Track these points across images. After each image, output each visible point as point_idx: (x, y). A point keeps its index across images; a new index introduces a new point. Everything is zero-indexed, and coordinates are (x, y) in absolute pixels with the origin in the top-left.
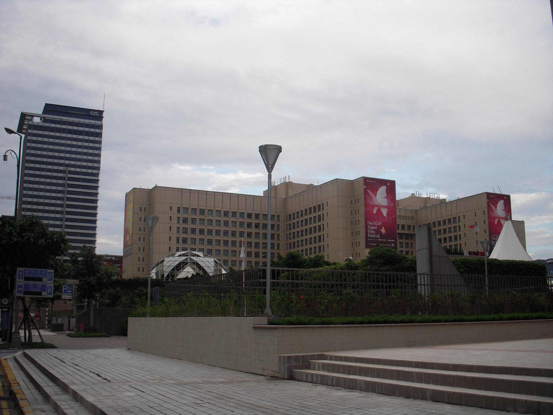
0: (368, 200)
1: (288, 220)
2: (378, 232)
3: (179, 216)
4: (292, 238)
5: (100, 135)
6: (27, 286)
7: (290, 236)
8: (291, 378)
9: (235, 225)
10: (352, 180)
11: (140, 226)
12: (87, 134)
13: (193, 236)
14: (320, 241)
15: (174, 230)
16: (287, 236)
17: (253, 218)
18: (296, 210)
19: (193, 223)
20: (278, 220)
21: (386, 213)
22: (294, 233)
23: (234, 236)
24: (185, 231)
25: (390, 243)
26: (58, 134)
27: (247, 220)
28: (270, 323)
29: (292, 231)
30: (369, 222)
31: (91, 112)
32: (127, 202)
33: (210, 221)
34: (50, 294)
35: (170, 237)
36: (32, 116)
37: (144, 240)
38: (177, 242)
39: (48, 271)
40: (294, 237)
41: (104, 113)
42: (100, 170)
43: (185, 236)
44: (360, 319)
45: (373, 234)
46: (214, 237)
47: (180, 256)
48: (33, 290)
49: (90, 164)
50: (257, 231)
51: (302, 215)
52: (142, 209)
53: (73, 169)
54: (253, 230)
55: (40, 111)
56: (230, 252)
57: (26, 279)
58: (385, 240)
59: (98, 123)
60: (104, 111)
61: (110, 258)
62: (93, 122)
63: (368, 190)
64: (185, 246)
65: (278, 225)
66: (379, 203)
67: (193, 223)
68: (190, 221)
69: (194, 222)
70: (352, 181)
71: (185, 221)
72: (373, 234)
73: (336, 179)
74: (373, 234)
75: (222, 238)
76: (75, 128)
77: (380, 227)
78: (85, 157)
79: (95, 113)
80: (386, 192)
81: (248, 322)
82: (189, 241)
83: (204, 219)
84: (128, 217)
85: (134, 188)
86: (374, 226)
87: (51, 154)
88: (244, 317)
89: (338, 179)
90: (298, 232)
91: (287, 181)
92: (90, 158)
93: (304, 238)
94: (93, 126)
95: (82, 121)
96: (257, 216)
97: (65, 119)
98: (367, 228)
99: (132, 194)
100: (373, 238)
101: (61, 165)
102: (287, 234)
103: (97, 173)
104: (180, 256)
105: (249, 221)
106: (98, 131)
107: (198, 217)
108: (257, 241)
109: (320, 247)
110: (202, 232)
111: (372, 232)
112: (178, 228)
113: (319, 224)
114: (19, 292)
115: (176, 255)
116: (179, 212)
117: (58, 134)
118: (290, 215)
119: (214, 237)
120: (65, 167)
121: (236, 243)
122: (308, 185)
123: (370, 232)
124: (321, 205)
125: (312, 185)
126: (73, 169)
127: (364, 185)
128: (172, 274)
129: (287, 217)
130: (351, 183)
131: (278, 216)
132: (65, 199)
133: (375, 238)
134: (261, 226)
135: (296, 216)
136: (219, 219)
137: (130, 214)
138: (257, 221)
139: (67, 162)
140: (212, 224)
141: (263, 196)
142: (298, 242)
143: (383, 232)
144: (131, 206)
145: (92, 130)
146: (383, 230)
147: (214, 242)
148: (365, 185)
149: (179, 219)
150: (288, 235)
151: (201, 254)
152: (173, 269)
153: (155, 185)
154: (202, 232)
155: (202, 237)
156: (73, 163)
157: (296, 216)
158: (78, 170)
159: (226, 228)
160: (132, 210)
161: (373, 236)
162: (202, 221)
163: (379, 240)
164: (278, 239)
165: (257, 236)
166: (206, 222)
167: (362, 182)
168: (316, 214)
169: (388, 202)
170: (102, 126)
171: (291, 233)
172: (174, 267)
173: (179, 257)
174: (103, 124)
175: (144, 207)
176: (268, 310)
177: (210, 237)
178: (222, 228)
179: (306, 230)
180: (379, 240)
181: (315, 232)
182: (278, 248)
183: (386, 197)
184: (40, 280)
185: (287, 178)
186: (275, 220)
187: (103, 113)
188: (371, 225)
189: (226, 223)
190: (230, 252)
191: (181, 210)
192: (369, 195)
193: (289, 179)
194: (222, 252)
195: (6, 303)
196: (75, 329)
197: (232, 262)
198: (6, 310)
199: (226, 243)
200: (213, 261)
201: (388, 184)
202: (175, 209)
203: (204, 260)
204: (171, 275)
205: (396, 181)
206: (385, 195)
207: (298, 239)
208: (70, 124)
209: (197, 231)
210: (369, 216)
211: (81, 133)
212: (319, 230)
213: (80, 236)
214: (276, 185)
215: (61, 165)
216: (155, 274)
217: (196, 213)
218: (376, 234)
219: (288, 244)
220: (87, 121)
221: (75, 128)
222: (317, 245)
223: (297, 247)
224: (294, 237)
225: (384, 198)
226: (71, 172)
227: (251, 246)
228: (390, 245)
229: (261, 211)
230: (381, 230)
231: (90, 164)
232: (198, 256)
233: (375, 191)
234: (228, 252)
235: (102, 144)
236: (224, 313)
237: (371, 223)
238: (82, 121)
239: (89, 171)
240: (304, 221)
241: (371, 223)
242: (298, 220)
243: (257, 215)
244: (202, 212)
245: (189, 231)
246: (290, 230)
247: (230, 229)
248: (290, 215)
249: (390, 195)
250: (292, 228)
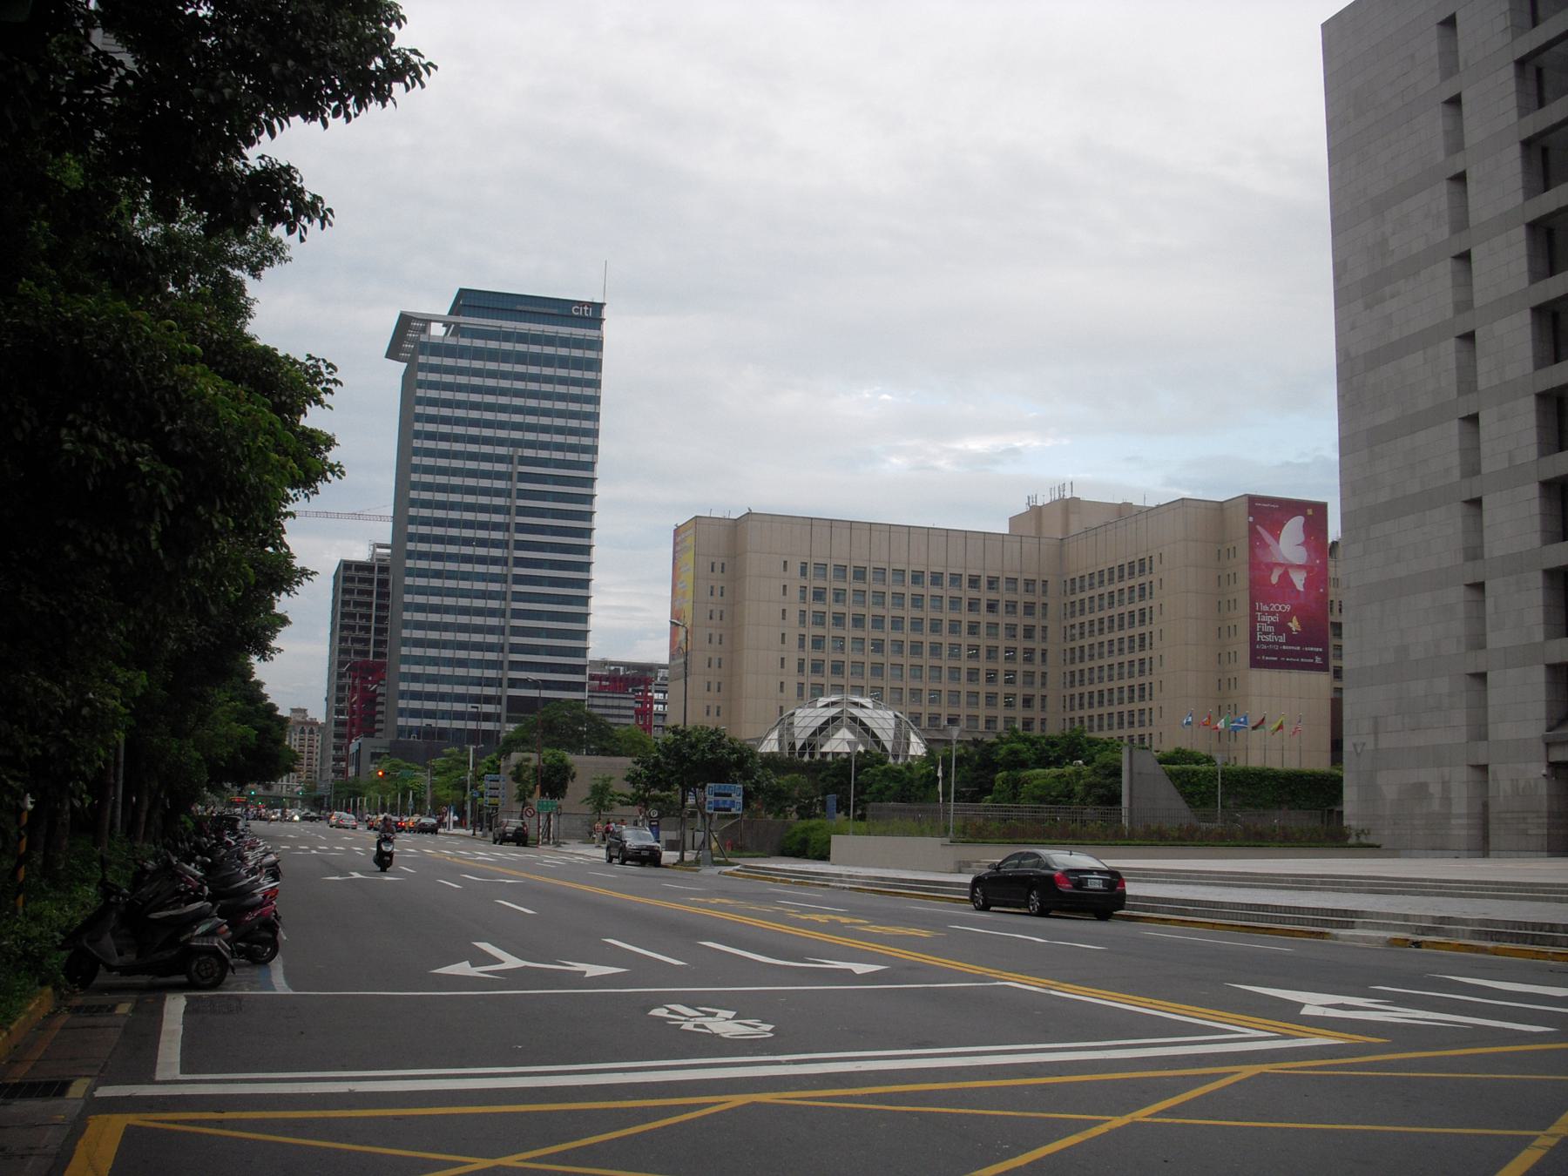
2: (1281, 627)
4: (1077, 636)
6: (717, 802)
7: (1073, 631)
8: (960, 872)
11: (711, 607)
12: (564, 362)
13: (838, 632)
14: (1142, 646)
15: (793, 616)
17: (982, 588)
20: (1045, 592)
21: (1303, 582)
22: (1082, 625)
23: (937, 632)
25: (1312, 655)
27: (968, 593)
28: (951, 842)
29: (1077, 620)
30: (1260, 606)
31: (574, 308)
32: (678, 548)
33: (880, 597)
34: (739, 809)
36: (427, 321)
41: (605, 307)
42: (597, 453)
43: (819, 631)
44: (1008, 841)
46: (888, 635)
47: (827, 706)
48: (722, 806)
50: (992, 618)
53: (529, 453)
54: (984, 617)
55: (444, 310)
56: (926, 671)
57: (716, 795)
58: (1298, 648)
59: (590, 333)
60: (605, 304)
61: (612, 668)
64: (837, 680)
68: (830, 596)
69: (841, 597)
70: (1222, 503)
71: (819, 595)
72: (1269, 633)
73: (1183, 499)
75: (907, 636)
77: (1286, 617)
78: (559, 422)
79: (583, 310)
80: (1304, 531)
81: (938, 840)
82: (828, 643)
83: (865, 591)
84: (680, 586)
85: (697, 517)
86: (1273, 614)
87: (474, 414)
88: (1143, 748)
91: (1068, 496)
92: (574, 423)
95: (550, 330)
96: (992, 583)
97: (509, 325)
98: (1253, 620)
100: (1268, 643)
102: (1065, 627)
103: (591, 460)
104: (827, 706)
105: (973, 594)
106: (590, 354)
107: (850, 585)
108: (992, 643)
109: (1142, 662)
110: (858, 621)
112: (803, 613)
113: (1142, 605)
114: (709, 808)
117: (492, 366)
118: (1073, 580)
119: (888, 635)
120: (511, 446)
122: (1120, 505)
123: (1261, 629)
125: (1127, 506)
126: (529, 453)
128: (810, 746)
130: (1219, 509)
131: (1045, 582)
133: (1274, 643)
134: (1001, 607)
135: (1087, 583)
137: (688, 578)
139: (516, 435)
140: (884, 604)
141: (1007, 532)
142: (1092, 646)
144: (688, 558)
145: (577, 353)
146: (1294, 625)
147: (888, 647)
148: (1250, 514)
150: (1068, 629)
152: (814, 734)
153: (748, 511)
154: (858, 621)
155: (859, 633)
157: (1087, 583)
158: (544, 454)
161: (1269, 638)
162: (860, 595)
164: (1044, 638)
165: (993, 631)
166: (869, 598)
167: (1244, 508)
168: (1135, 582)
169: (1309, 555)
170: (602, 342)
171: (1074, 625)
174: (602, 338)
176: (951, 833)
177: (877, 634)
178: (909, 613)
179: (1111, 619)
181: (1132, 624)
182: (1044, 660)
183: (1305, 543)
184: (730, 795)
185: (1068, 487)
186: (1037, 592)
188: (1264, 613)
189: (917, 601)
190: (926, 670)
191: (810, 570)
192: (1262, 540)
195: (656, 815)
196: (209, 860)
197: (930, 695)
198: (656, 823)
199: (916, 648)
200: (893, 716)
201: (1310, 512)
202: (795, 569)
203: (875, 715)
206: (1301, 538)
208: (522, 338)
210: (1260, 591)
211: (549, 361)
213: (548, 620)
216: (777, 743)
219: (1068, 651)
220: (564, 331)
222: (1137, 656)
226: (525, 461)
227: (977, 656)
228: (1312, 661)
232: (863, 706)
233: (1276, 529)
234: (921, 670)
235: (602, 387)
236: (922, 834)
237: (1266, 608)
238: (550, 330)
240: (1106, 596)
241: (1266, 608)
242: (1091, 593)
244: (860, 574)
245: (829, 619)
246: (1072, 617)
247: (928, 613)
249: (1312, 538)
250: (1077, 613)
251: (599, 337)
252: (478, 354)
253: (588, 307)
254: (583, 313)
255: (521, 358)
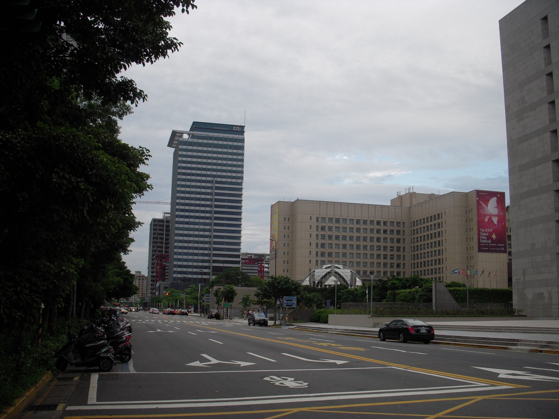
0: (481, 211)
1: (412, 226)
2: (489, 237)
3: (318, 224)
4: (416, 242)
5: (242, 148)
8: (375, 327)
9: (365, 231)
10: (467, 192)
13: (330, 242)
16: (411, 240)
18: (419, 217)
19: (329, 230)
20: (404, 226)
21: (497, 221)
22: (417, 238)
24: (323, 237)
26: (205, 149)
27: (376, 227)
28: (371, 316)
29: (416, 236)
34: (295, 306)
35: (310, 243)
36: (182, 133)
37: (288, 245)
38: (316, 247)
39: (295, 297)
40: (417, 241)
41: (245, 127)
43: (323, 241)
45: (485, 239)
46: (348, 242)
47: (326, 268)
49: (234, 175)
50: (385, 236)
51: (424, 222)
52: (286, 218)
55: (188, 129)
57: (287, 300)
59: (240, 137)
61: (250, 256)
62: (236, 136)
63: (480, 202)
65: (404, 231)
66: (490, 213)
67: (329, 230)
68: (327, 229)
69: (331, 229)
71: (323, 228)
74: (485, 239)
76: (220, 142)
77: (491, 234)
79: (237, 128)
81: (367, 316)
82: (327, 246)
83: (339, 227)
85: (279, 201)
86: (486, 232)
89: (454, 192)
90: (421, 237)
91: (411, 192)
93: (426, 242)
94: (236, 148)
95: (226, 135)
96: (385, 223)
97: (211, 134)
98: (479, 235)
99: (277, 206)
100: (485, 243)
101: (209, 176)
105: (378, 227)
106: (240, 144)
107: (334, 225)
109: (439, 250)
110: (337, 238)
111: (484, 238)
112: (317, 235)
114: (285, 305)
115: (324, 268)
116: (318, 221)
117: (205, 149)
118: (414, 222)
119: (348, 242)
121: (367, 247)
123: (482, 238)
124: (440, 215)
127: (477, 197)
128: (320, 282)
129: (411, 224)
131: (404, 223)
132: (213, 206)
136: (352, 226)
137: (276, 223)
138: (385, 228)
139: (214, 173)
141: (390, 205)
143: (494, 238)
146: (494, 236)
148: (477, 197)
149: (318, 227)
150: (412, 239)
151: (341, 266)
152: (322, 278)
153: (297, 199)
155: (337, 242)
156: (219, 173)
158: (224, 180)
159: (358, 234)
160: (278, 220)
161: (485, 241)
163: (490, 245)
165: (386, 240)
169: (499, 211)
170: (244, 140)
171: (415, 238)
172: (322, 276)
173: (326, 269)
175: (287, 217)
177: (344, 242)
178: (355, 234)
180: (490, 245)
182: (404, 251)
183: (497, 207)
184: (292, 301)
185: (411, 188)
187: (244, 127)
188: (483, 232)
189: (358, 230)
191: (320, 220)
192: (481, 206)
193: (413, 190)
194: (355, 255)
196: (106, 326)
198: (266, 311)
201: (499, 196)
202: (314, 220)
203: (344, 271)
204: (320, 282)
205: (505, 193)
207: (421, 243)
209: (334, 238)
210: (481, 224)
212: (438, 236)
214: (401, 195)
215: (209, 176)
217: (332, 222)
218: (488, 239)
219: (413, 247)
220: (231, 136)
221: (220, 142)
222: (437, 249)
223: (420, 250)
224: (417, 241)
225: (495, 208)
226: (217, 182)
227: (380, 249)
228: (500, 249)
229: (389, 219)
230: (492, 236)
231: (234, 175)
232: (339, 268)
233: (486, 202)
237: (483, 230)
238: (226, 135)
239: (234, 180)
241: (483, 230)
243: (385, 223)
244: (338, 221)
245: (327, 237)
247: (362, 234)
248: (414, 222)
250: (416, 234)
251: (243, 138)
252: (200, 145)
253: (239, 127)
254: (237, 129)
255: (216, 146)
